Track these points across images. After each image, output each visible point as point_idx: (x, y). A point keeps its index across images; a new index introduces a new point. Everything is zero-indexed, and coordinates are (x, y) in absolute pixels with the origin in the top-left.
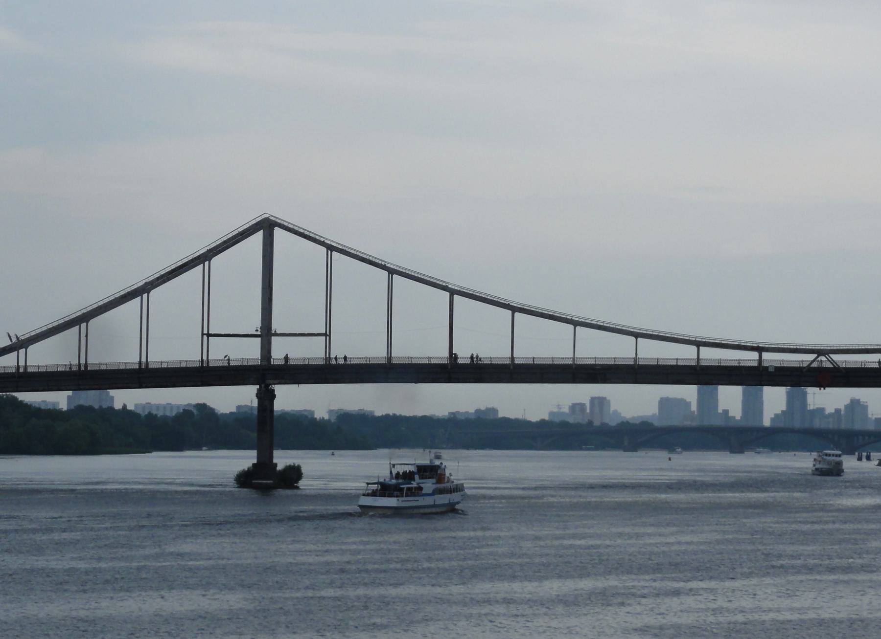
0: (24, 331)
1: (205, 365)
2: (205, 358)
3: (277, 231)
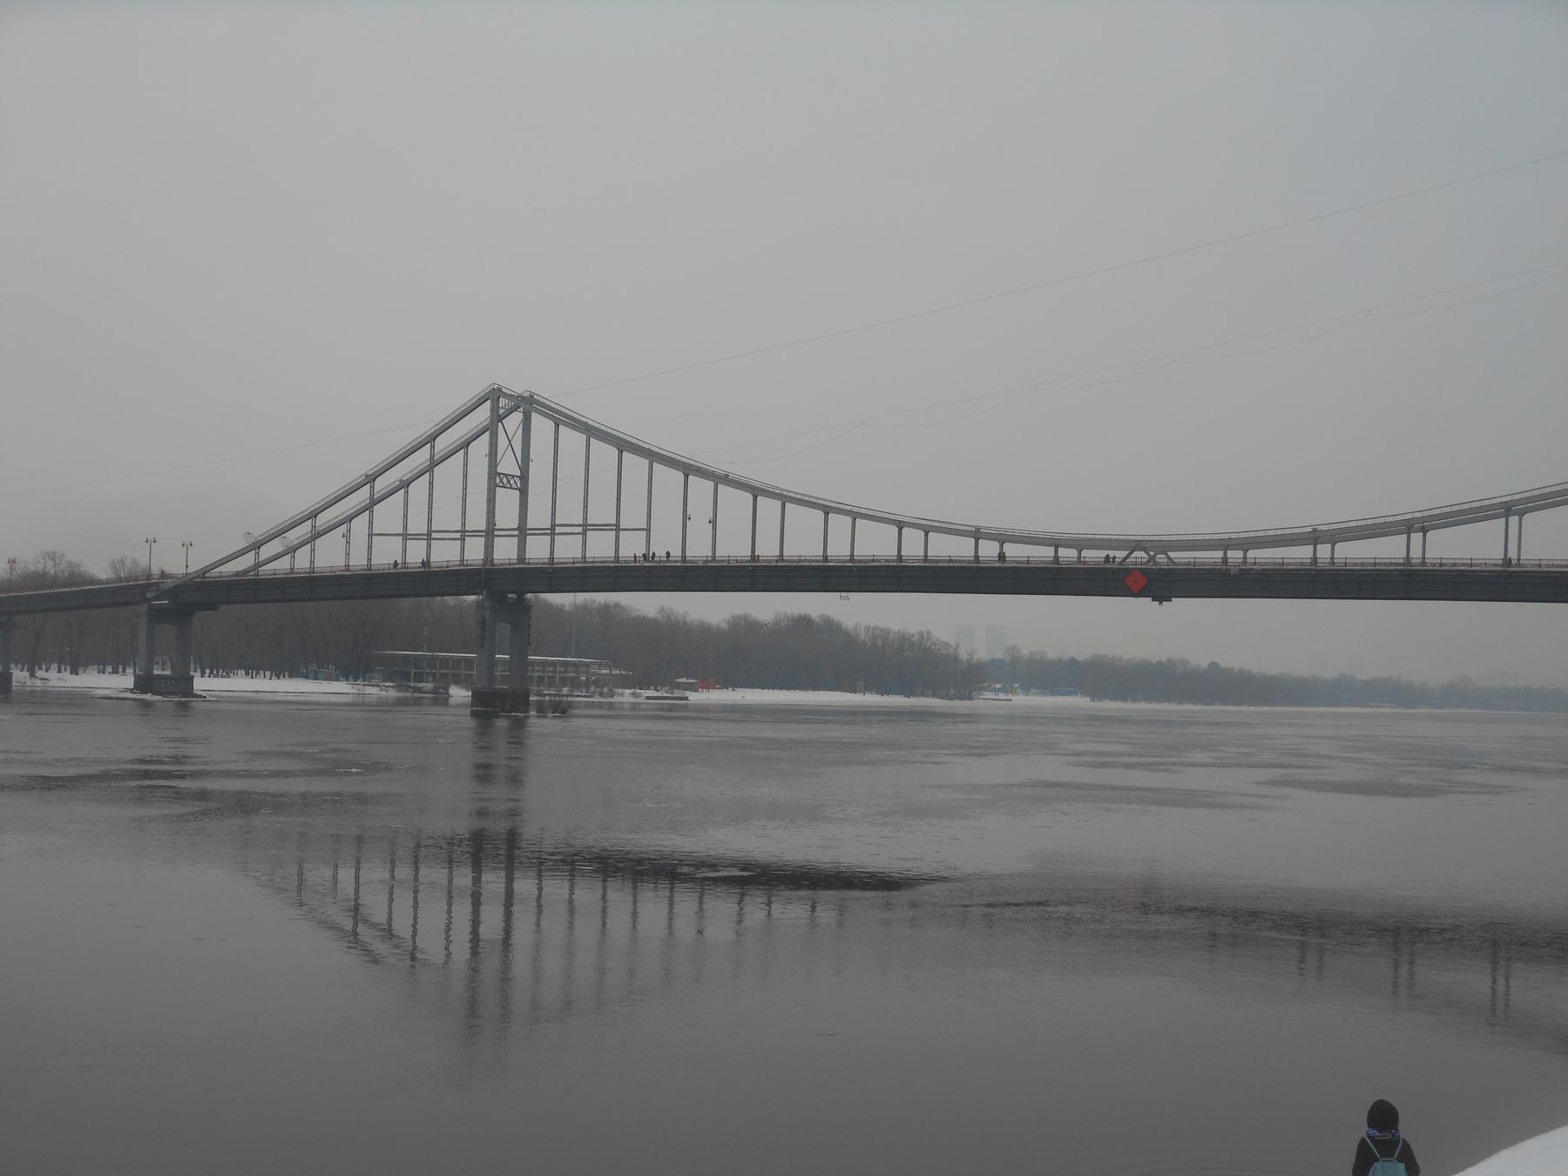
0: (258, 532)
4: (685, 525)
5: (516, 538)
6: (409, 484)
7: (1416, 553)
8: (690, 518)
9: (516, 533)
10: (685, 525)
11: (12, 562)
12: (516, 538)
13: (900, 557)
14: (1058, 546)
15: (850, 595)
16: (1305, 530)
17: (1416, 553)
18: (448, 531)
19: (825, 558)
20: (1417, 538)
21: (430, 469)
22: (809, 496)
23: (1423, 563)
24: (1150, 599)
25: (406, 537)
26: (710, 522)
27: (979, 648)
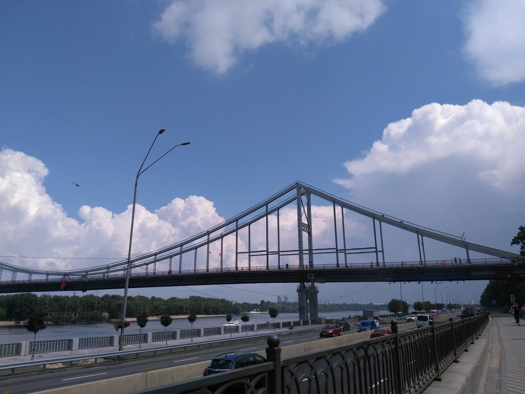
1: (381, 265)
4: (208, 255)
5: (308, 255)
6: (223, 237)
7: (342, 262)
8: (210, 253)
9: (314, 252)
10: (208, 255)
11: (287, 265)
12: (308, 255)
13: (208, 270)
14: (382, 252)
15: (444, 282)
16: (105, 266)
17: (342, 262)
18: (288, 251)
19: (180, 271)
20: (308, 252)
21: (236, 230)
22: (188, 247)
23: (384, 265)
24: (132, 297)
25: (337, 251)
26: (220, 255)
27: (296, 367)
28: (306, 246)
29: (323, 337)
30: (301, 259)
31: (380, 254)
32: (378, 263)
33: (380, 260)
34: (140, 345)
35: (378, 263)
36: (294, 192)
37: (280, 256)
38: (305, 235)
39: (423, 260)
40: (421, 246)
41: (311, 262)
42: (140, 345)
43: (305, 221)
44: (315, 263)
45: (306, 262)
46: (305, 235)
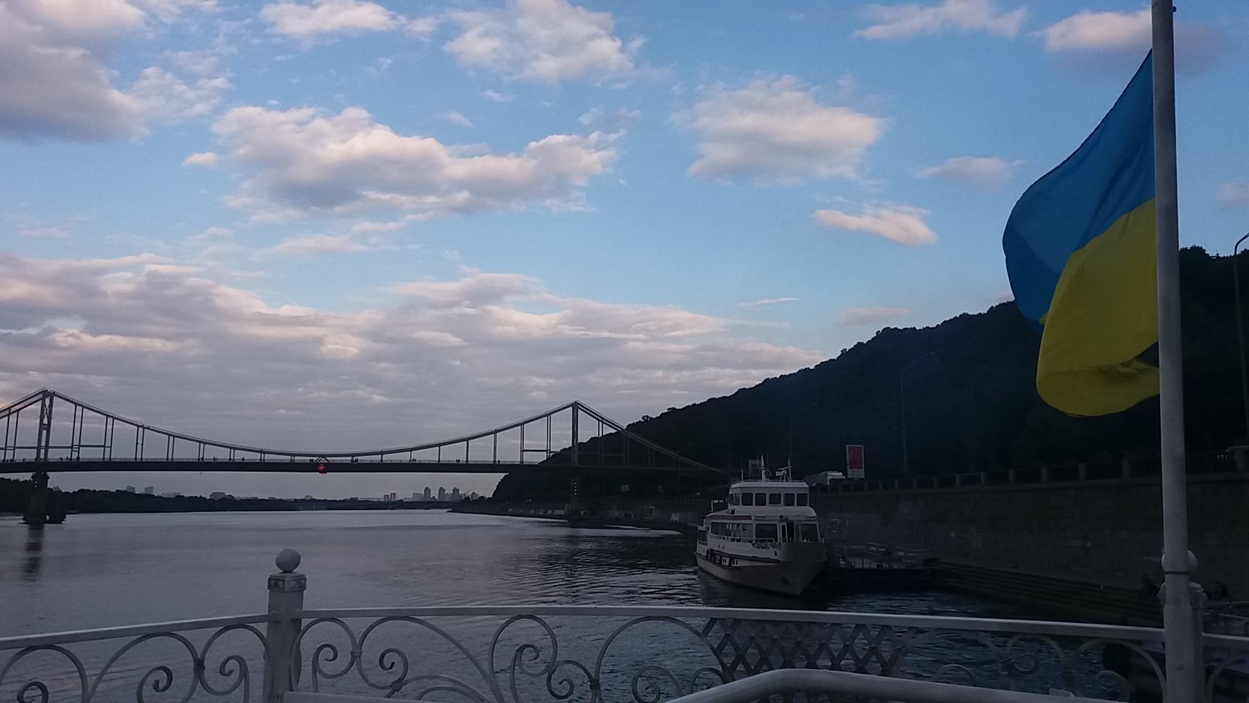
2: (170, 457)
3: (55, 398)
17: (75, 456)
28: (43, 444)
29: (829, 625)
30: (38, 453)
31: (108, 450)
32: (167, 459)
33: (107, 456)
34: (1168, 573)
35: (167, 459)
36: (41, 396)
37: (36, 446)
38: (44, 432)
39: (232, 457)
40: (140, 442)
41: (46, 455)
42: (1168, 573)
43: (45, 421)
44: (49, 457)
45: (42, 456)
46: (44, 432)
